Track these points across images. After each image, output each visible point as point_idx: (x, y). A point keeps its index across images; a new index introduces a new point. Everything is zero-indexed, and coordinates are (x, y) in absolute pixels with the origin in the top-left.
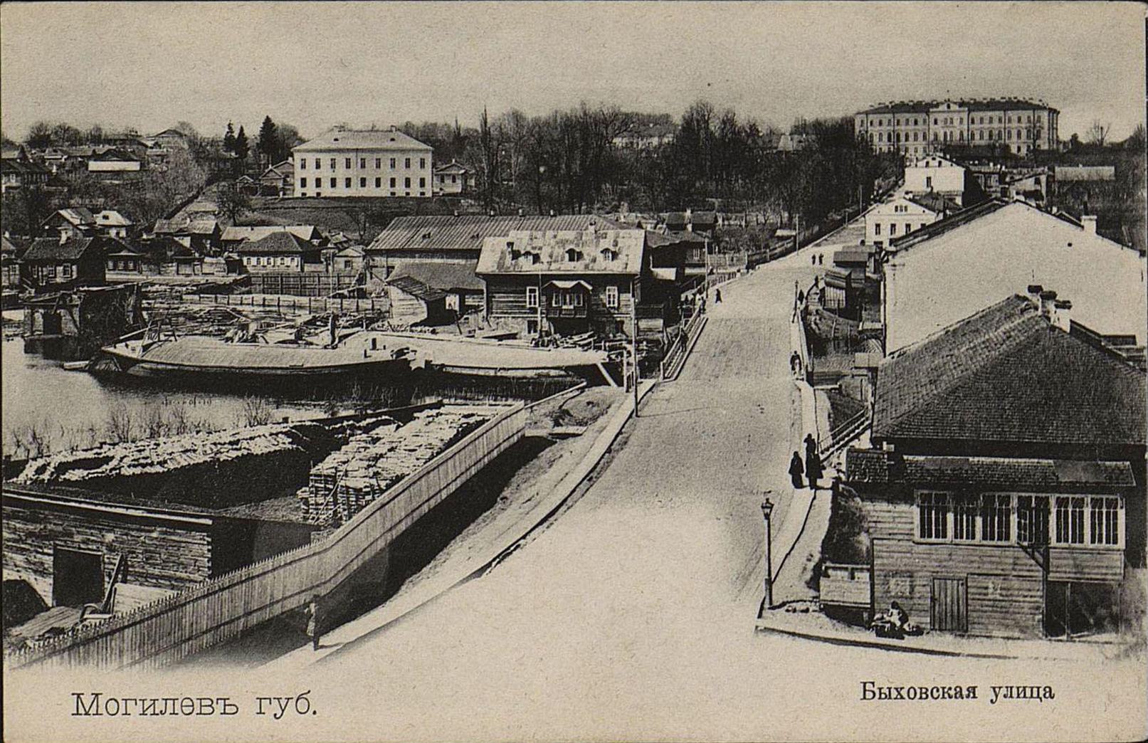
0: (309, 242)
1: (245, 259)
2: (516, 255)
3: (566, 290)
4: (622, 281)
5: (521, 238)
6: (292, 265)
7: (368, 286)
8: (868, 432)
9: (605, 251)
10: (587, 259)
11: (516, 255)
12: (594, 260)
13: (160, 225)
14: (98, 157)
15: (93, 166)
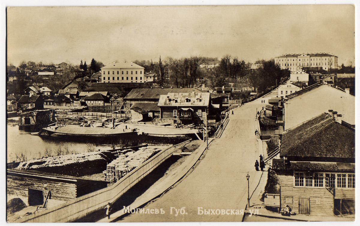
0: (106, 96)
1: (86, 102)
2: (170, 100)
3: (185, 111)
4: (203, 108)
5: (171, 95)
6: (101, 103)
7: (124, 110)
8: (279, 154)
9: (198, 99)
10: (192, 101)
11: (170, 100)
12: (194, 102)
13: (61, 91)
14: (41, 71)
15: (40, 73)
